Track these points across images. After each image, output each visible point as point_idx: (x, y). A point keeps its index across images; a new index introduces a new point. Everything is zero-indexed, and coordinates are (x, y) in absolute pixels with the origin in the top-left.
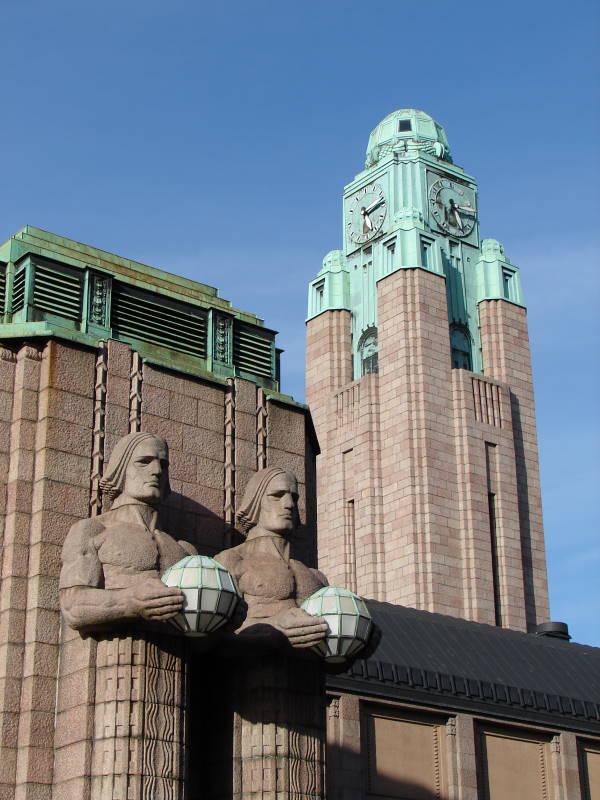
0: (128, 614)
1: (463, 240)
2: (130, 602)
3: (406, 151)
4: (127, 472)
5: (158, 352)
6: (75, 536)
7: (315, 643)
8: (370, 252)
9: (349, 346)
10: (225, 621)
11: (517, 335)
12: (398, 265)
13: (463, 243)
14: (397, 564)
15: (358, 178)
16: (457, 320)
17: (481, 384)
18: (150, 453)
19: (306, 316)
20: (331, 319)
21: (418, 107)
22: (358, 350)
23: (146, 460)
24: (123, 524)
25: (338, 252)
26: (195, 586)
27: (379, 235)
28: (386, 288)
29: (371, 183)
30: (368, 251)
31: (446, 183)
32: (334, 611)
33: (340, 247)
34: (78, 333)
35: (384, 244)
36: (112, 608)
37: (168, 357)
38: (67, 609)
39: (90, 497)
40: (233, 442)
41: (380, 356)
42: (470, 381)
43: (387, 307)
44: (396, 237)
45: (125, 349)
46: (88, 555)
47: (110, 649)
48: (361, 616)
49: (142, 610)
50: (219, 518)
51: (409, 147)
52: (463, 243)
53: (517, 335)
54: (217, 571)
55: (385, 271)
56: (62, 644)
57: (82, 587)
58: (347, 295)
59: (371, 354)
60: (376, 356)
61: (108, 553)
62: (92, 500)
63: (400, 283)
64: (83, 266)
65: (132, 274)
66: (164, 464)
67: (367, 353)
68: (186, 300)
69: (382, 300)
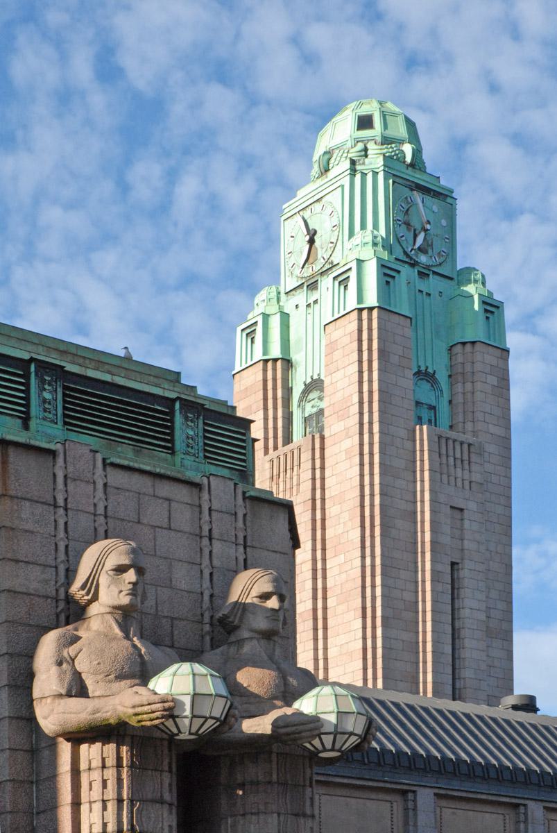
0: (112, 721)
1: (435, 269)
2: (115, 710)
3: (366, 156)
4: (100, 582)
5: (119, 449)
6: (48, 645)
7: (160, 720)
8: (316, 288)
10: (218, 723)
11: (496, 383)
13: (434, 273)
14: (342, 639)
15: (301, 193)
16: (423, 369)
17: (450, 443)
18: (127, 562)
20: (265, 370)
22: (299, 406)
23: (120, 570)
24: (98, 633)
26: (188, 693)
27: (327, 266)
28: (337, 332)
29: (318, 200)
30: (313, 286)
31: (417, 197)
32: (331, 709)
34: (29, 434)
35: (335, 278)
36: (95, 716)
37: (131, 455)
38: (45, 718)
39: (57, 607)
40: (66, 485)
41: (326, 413)
42: (436, 440)
43: (337, 354)
44: (350, 269)
45: (86, 450)
46: (65, 666)
47: (91, 753)
48: (338, 712)
49: (129, 717)
51: (369, 152)
52: (434, 273)
53: (496, 383)
54: (209, 677)
56: (37, 750)
57: (61, 696)
59: (315, 410)
60: (321, 412)
61: (82, 665)
62: (59, 609)
64: (26, 356)
65: (81, 361)
66: (140, 571)
67: (309, 410)
68: (147, 388)
69: (332, 347)
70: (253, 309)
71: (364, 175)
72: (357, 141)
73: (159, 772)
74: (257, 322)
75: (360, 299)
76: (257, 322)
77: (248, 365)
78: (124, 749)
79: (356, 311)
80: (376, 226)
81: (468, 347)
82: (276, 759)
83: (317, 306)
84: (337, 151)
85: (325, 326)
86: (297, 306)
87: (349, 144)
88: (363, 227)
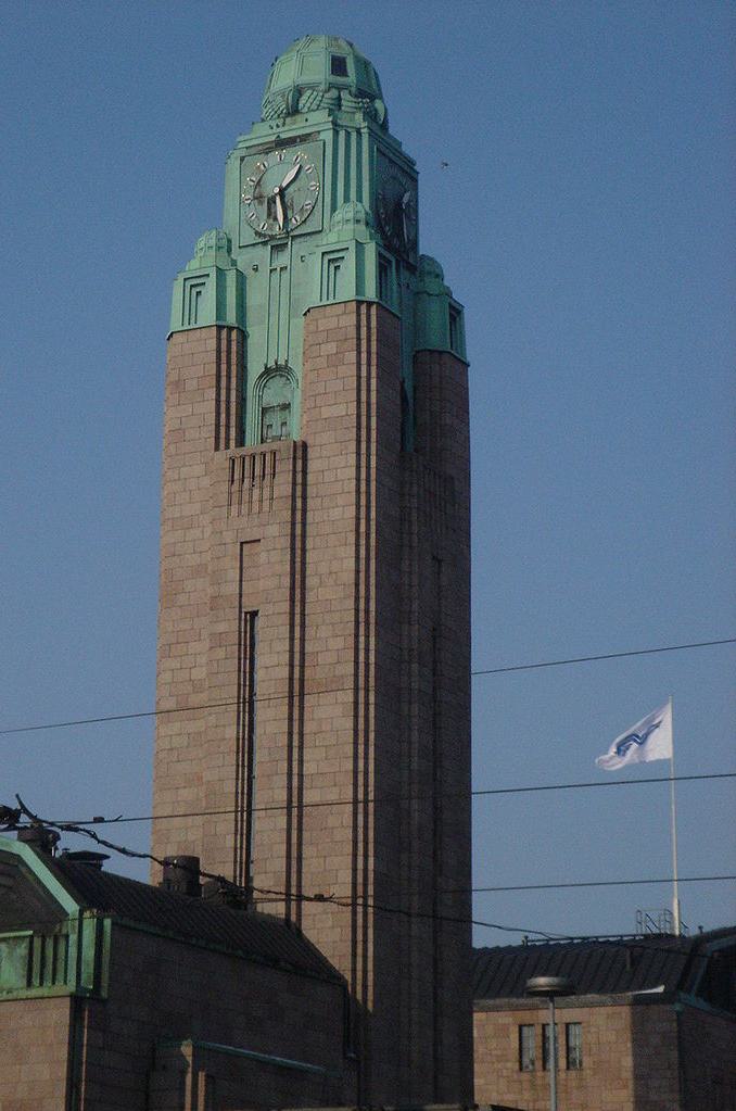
71: (348, 134)
72: (331, 86)
75: (360, 288)
77: (189, 327)
78: (107, 922)
79: (354, 303)
80: (360, 199)
81: (436, 355)
82: (716, 942)
83: (286, 275)
84: (310, 91)
87: (322, 87)
88: (347, 199)
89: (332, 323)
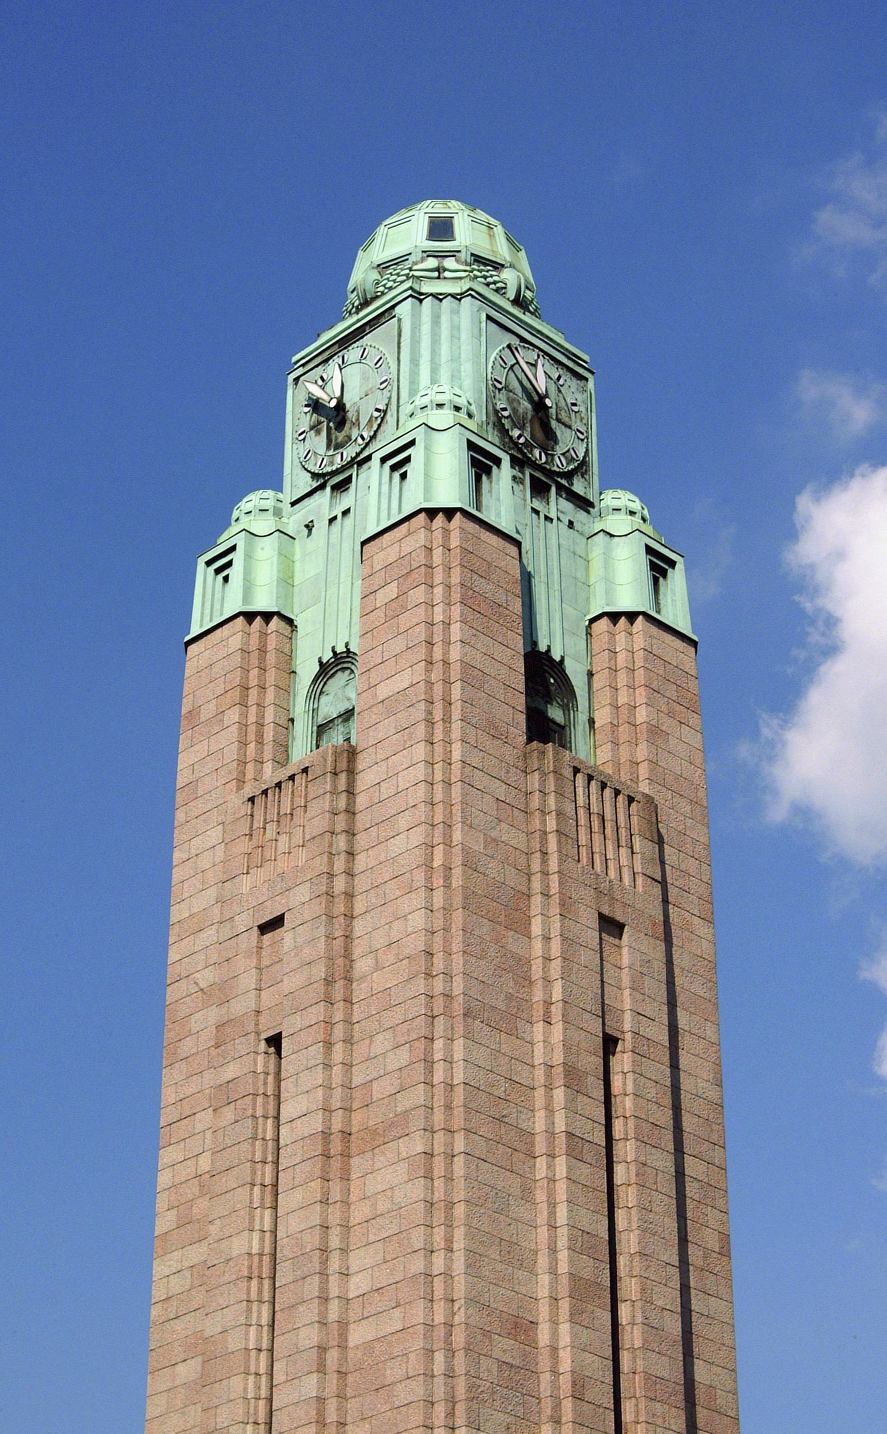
9: (286, 690)
12: (414, 500)
17: (608, 792)
19: (187, 626)
21: (473, 203)
25: (270, 493)
33: (278, 487)
50: (170, 902)
55: (384, 514)
58: (286, 581)
63: (236, 642)
67: (330, 707)
70: (229, 524)
73: (320, 1058)
74: (235, 546)
76: (235, 546)
83: (350, 520)
85: (363, 544)
86: (309, 527)
89: (392, 554)
